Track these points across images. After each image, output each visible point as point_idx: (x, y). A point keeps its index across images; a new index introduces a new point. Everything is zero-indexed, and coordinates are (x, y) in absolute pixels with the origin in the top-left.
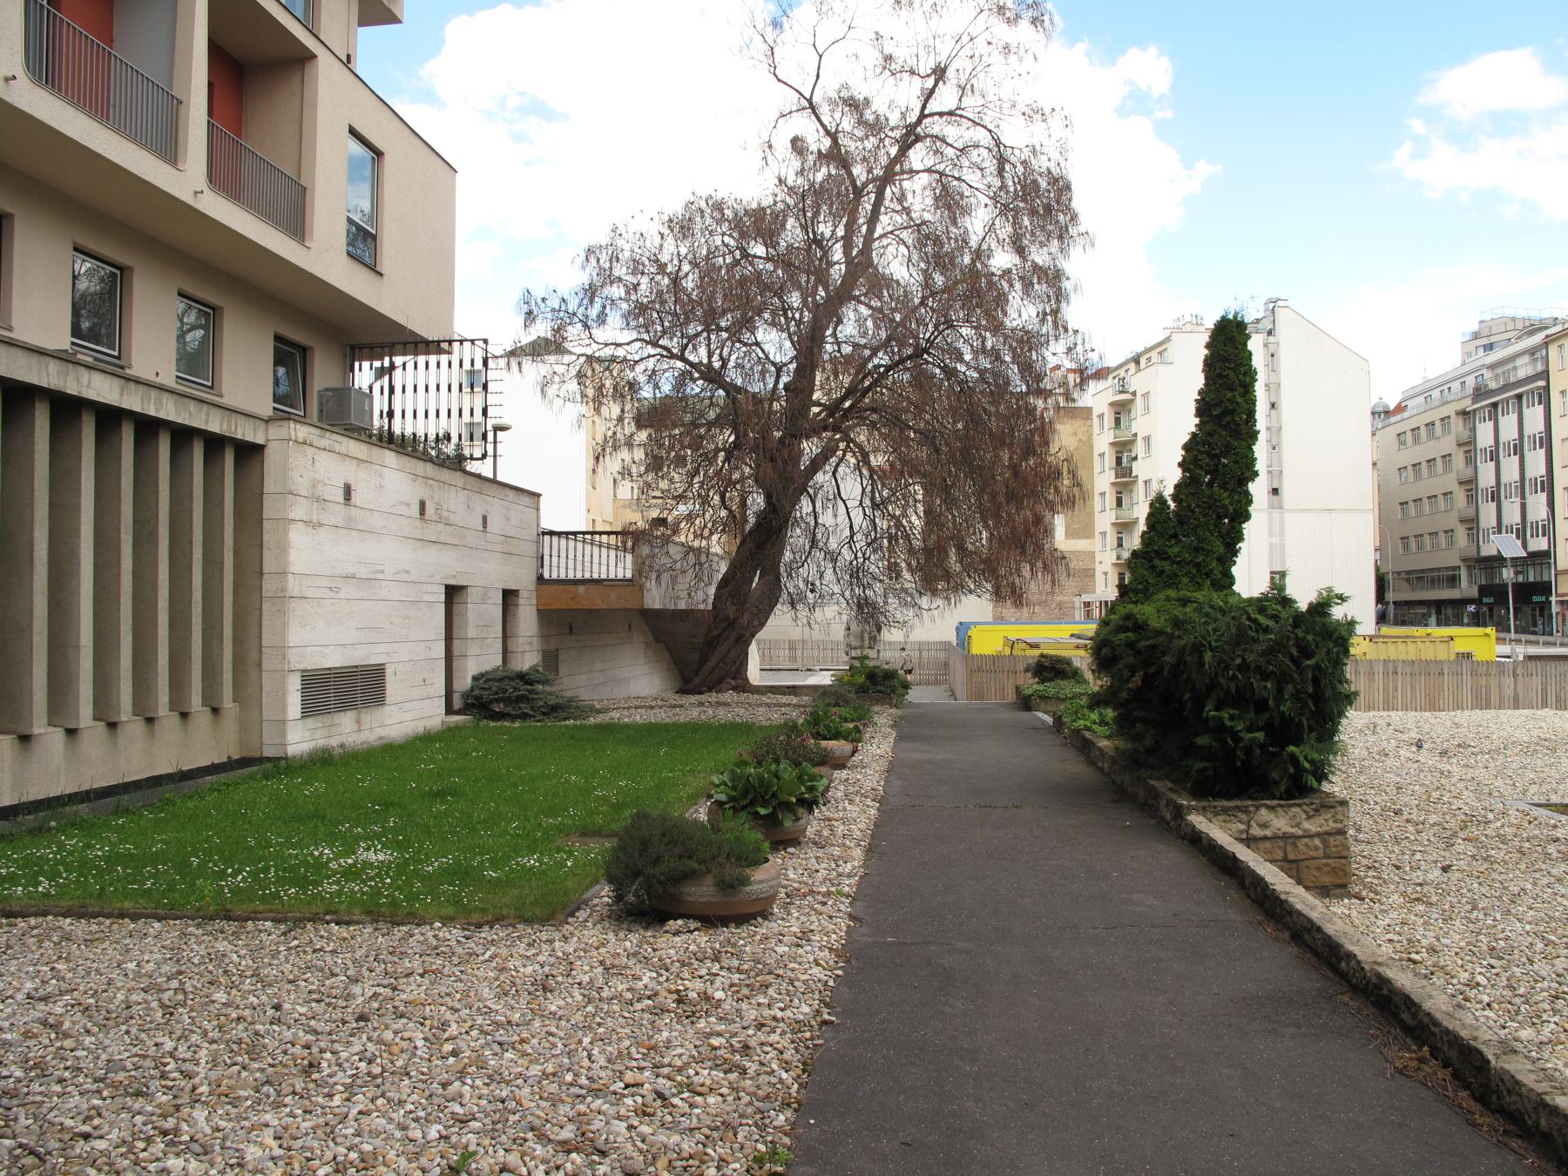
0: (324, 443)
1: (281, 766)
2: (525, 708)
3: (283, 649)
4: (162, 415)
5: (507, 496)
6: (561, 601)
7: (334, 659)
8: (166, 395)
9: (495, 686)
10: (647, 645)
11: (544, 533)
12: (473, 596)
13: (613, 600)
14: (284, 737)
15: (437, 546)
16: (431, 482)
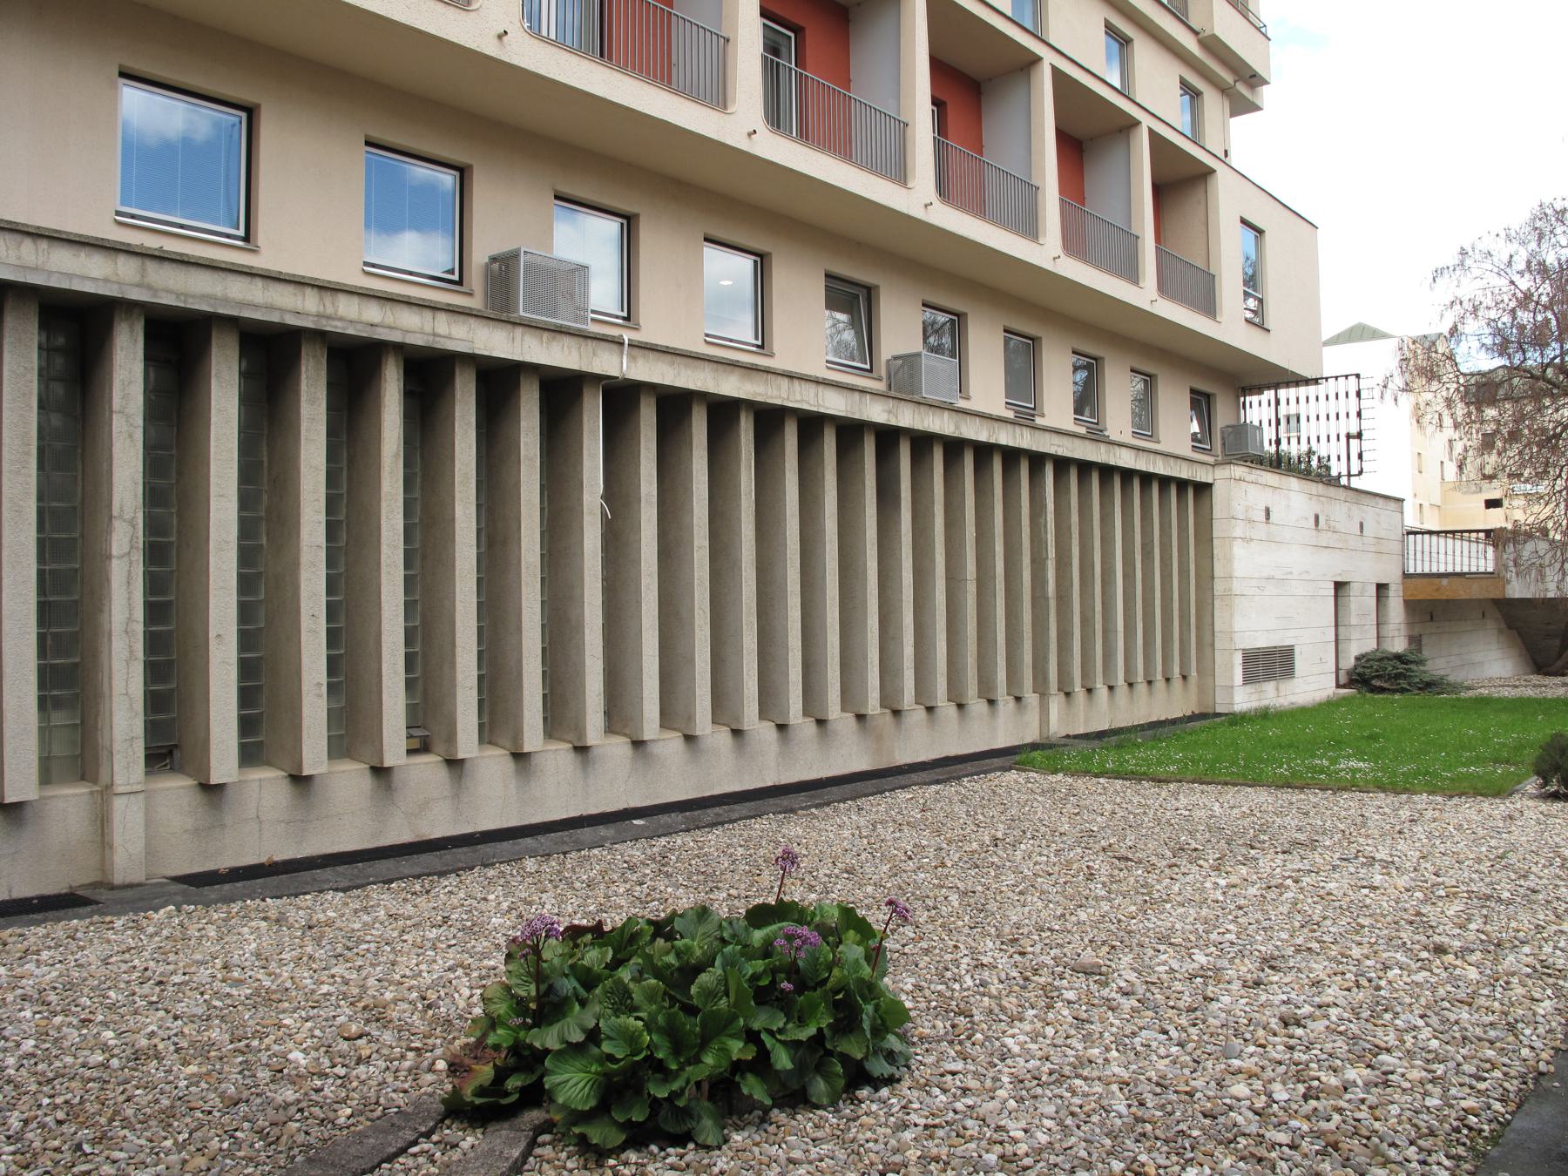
1: (1236, 719)
2: (1403, 684)
3: (1230, 634)
4: (1156, 472)
5: (1377, 503)
6: (1425, 592)
7: (1262, 642)
8: (1158, 456)
9: (1376, 665)
10: (1500, 631)
11: (1409, 533)
12: (1354, 589)
13: (1476, 591)
15: (1328, 550)
16: (1322, 499)
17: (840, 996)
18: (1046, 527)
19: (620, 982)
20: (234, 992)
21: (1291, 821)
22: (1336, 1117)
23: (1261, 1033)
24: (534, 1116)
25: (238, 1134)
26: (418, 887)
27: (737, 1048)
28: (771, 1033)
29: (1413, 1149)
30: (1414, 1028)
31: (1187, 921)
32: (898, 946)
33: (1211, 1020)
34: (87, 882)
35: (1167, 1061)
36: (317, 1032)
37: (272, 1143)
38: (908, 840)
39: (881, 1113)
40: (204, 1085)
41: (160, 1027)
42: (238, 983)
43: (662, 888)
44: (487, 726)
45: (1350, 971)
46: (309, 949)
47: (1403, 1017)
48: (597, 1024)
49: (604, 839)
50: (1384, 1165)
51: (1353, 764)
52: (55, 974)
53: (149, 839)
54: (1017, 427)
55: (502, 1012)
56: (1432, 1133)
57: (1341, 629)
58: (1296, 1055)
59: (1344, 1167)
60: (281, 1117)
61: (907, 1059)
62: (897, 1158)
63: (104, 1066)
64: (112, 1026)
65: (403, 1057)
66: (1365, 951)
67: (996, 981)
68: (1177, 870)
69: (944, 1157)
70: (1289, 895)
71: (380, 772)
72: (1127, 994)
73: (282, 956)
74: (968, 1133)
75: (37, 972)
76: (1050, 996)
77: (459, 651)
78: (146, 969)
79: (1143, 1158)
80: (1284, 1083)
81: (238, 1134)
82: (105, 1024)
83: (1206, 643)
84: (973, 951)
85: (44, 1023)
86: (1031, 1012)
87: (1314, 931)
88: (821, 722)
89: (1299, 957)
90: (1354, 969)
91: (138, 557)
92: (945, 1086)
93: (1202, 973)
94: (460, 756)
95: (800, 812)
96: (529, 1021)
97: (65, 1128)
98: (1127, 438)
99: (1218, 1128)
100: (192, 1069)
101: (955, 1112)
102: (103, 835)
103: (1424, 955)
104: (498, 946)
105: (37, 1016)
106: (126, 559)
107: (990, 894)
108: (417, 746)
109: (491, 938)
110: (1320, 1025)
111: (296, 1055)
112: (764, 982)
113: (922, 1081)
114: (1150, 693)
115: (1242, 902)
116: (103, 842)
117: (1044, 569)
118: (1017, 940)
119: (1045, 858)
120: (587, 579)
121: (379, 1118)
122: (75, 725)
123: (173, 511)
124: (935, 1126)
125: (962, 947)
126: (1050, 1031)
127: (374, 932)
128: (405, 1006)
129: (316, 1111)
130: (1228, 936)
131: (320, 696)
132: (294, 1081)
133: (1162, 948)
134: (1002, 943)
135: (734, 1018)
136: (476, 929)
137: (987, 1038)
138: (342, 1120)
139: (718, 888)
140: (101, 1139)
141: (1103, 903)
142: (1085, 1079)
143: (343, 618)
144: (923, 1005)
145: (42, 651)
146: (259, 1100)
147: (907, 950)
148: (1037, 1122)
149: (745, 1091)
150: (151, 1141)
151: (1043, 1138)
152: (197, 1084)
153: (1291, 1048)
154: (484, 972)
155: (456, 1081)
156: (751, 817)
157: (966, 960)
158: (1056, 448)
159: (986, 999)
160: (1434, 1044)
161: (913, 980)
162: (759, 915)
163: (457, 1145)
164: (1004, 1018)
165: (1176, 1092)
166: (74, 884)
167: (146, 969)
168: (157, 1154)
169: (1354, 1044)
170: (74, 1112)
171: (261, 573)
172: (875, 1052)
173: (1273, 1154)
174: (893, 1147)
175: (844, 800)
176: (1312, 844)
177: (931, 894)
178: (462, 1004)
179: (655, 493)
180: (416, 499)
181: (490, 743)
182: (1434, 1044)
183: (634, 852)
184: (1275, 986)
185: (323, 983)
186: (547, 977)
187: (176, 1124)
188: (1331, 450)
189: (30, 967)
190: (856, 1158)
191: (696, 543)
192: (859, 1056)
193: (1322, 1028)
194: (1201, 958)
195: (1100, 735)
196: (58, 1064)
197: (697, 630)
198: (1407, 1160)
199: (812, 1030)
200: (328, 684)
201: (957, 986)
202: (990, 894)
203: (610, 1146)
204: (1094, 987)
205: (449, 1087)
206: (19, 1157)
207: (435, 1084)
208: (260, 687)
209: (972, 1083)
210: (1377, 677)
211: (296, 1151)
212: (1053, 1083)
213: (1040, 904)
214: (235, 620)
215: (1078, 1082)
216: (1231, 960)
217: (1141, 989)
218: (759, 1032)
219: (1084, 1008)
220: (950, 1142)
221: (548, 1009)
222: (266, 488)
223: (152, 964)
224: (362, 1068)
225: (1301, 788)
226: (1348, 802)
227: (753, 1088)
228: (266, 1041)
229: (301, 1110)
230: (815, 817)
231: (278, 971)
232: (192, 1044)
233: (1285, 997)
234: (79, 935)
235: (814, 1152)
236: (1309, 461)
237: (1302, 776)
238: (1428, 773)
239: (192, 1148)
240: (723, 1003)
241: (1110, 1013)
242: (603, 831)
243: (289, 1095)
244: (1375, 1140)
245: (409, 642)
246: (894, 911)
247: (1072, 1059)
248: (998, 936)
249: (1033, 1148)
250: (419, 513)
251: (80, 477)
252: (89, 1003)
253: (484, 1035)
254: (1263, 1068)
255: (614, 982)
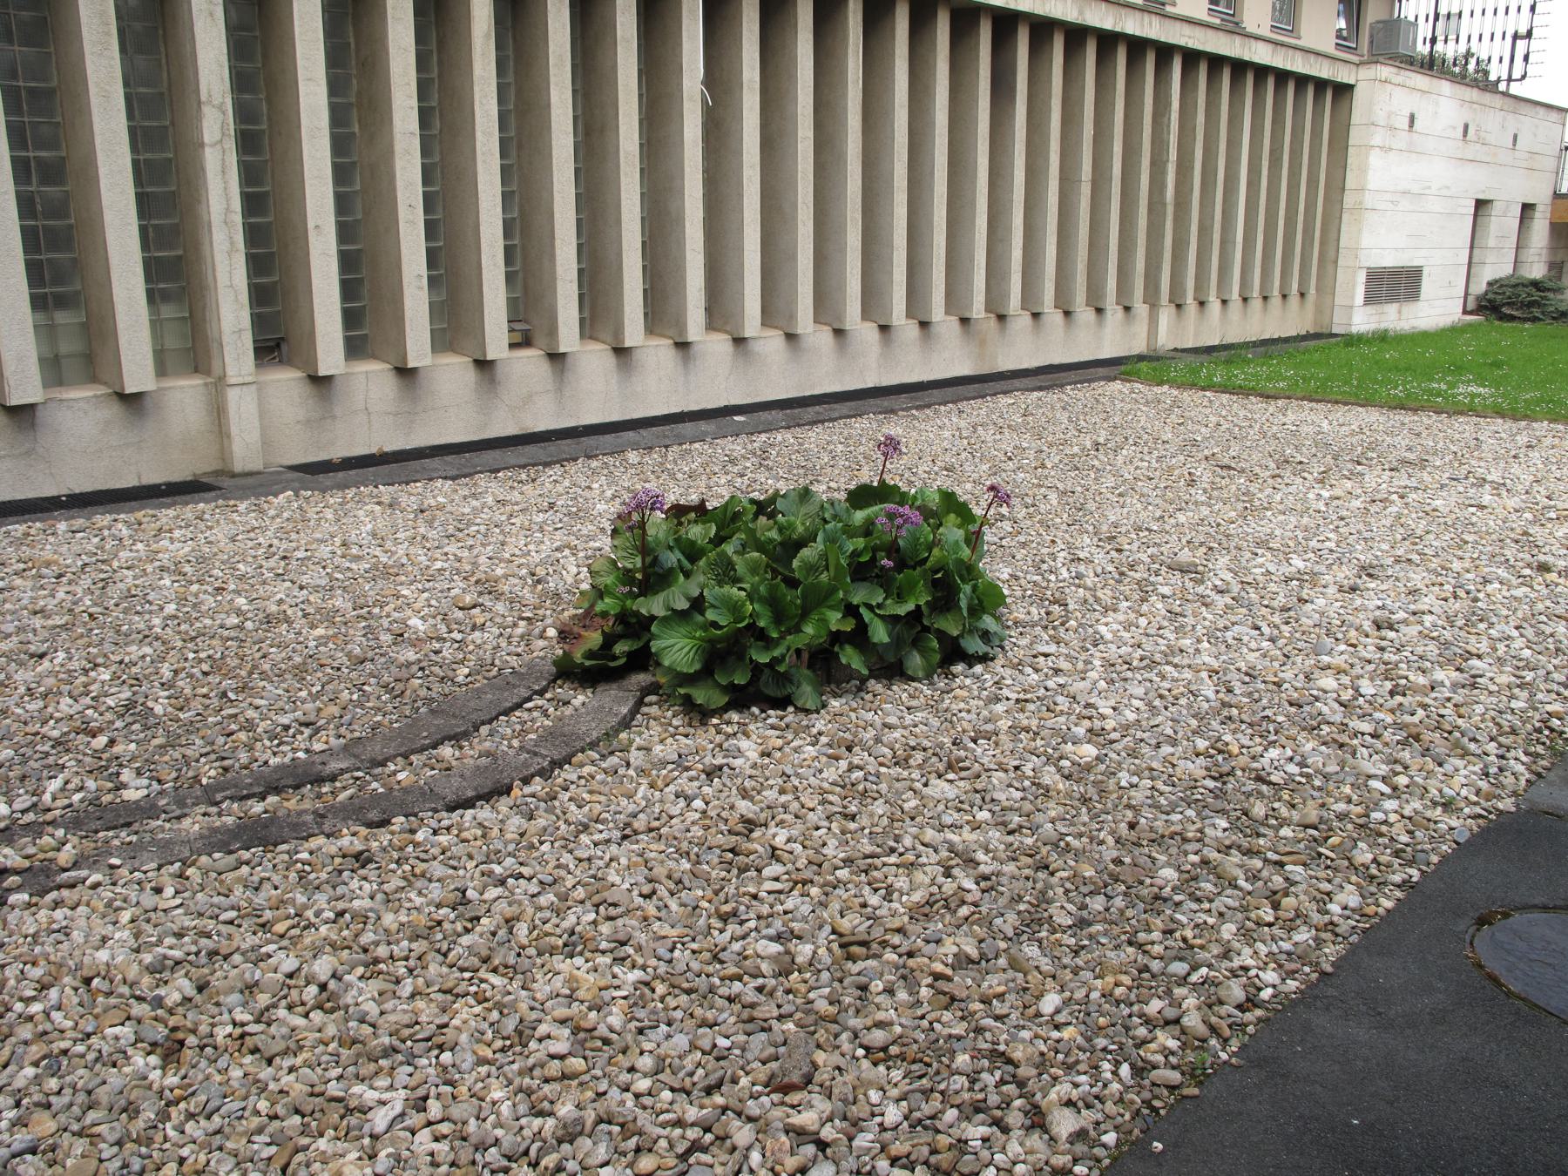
0: (1399, 79)
1: (1351, 340)
2: (1536, 312)
3: (1355, 252)
4: (1294, 69)
7: (1389, 261)
9: (1509, 291)
12: (1497, 209)
14: (1350, 318)
17: (939, 575)
18: (1169, 126)
19: (724, 553)
20: (354, 566)
21: (1402, 441)
22: (1421, 713)
23: (1353, 633)
24: (642, 679)
25: (366, 688)
26: (524, 476)
27: (835, 620)
28: (870, 607)
29: (1493, 744)
30: (1509, 638)
31: (1287, 528)
32: (996, 539)
33: (1304, 620)
34: (209, 470)
35: (1257, 654)
36: (433, 602)
37: (398, 696)
38: (1008, 442)
39: (975, 687)
40: (331, 645)
41: (288, 596)
42: (357, 558)
43: (763, 480)
44: (588, 322)
45: (1448, 583)
46: (422, 530)
47: (1497, 627)
48: (702, 593)
49: (706, 434)
50: (1462, 757)
51: (1473, 389)
52: (187, 549)
53: (264, 429)
54: (1146, 14)
55: (609, 582)
56: (1514, 732)
57: (1476, 251)
58: (1386, 656)
59: (1423, 756)
60: (404, 674)
61: (1002, 640)
62: (989, 727)
63: (240, 627)
64: (243, 594)
65: (515, 625)
66: (1467, 565)
67: (1092, 575)
68: (1279, 480)
69: (1034, 728)
70: (1393, 509)
71: (484, 365)
72: (1221, 592)
73: (398, 536)
74: (1058, 708)
75: (171, 547)
76: (1145, 591)
77: (558, 243)
78: (271, 546)
79: (1227, 738)
80: (1372, 679)
81: (366, 688)
82: (238, 592)
83: (1329, 261)
84: (1070, 547)
85: (182, 590)
86: (1126, 604)
87: (1416, 544)
88: (924, 325)
89: (1397, 567)
90: (1453, 581)
91: (231, 145)
92: (1038, 666)
93: (1300, 577)
94: (562, 350)
95: (900, 413)
96: (635, 590)
97: (210, 678)
98: (1265, 31)
99: (1303, 716)
100: (320, 631)
101: (1047, 689)
102: (220, 425)
103: (1527, 572)
104: (603, 530)
105: (176, 584)
106: (218, 147)
107: (1089, 495)
108: (520, 340)
109: (596, 522)
110: (1413, 630)
111: (415, 622)
112: (865, 558)
113: (1016, 661)
114: (1265, 309)
115: (1345, 513)
116: (221, 432)
117: (1164, 173)
118: (1115, 537)
119: (1146, 464)
120: (687, 170)
121: (495, 677)
122: (184, 318)
123: (261, 96)
124: (1026, 701)
125: (1059, 542)
126: (1143, 622)
127: (483, 516)
128: (515, 581)
129: (436, 669)
130: (1327, 544)
131: (421, 288)
132: (416, 643)
133: (1260, 551)
134: (1100, 540)
135: (834, 590)
136: (582, 514)
137: (1081, 625)
138: (460, 679)
139: (818, 481)
140: (242, 689)
141: (1203, 508)
142: (1176, 666)
143: (440, 210)
144: (1019, 593)
145: (145, 245)
146: (383, 660)
147: (1004, 542)
148: (1126, 701)
149: (844, 661)
150: (288, 691)
151: (1132, 716)
152: (325, 645)
153: (1382, 649)
154: (590, 553)
155: (566, 647)
156: (854, 416)
157: (1063, 554)
158: (1186, 39)
159: (1081, 590)
160: (1527, 653)
161: (1010, 571)
162: (862, 496)
163: (569, 703)
164: (1098, 608)
165: (1264, 682)
166: (198, 472)
167: (271, 546)
168: (294, 702)
169: (1446, 649)
170: (217, 665)
171: (355, 163)
172: (970, 632)
173: (1355, 742)
174: (985, 718)
175: (945, 403)
176: (1423, 463)
177: (1030, 493)
178: (570, 580)
179: (758, 79)
180: (509, 84)
181: (591, 338)
182: (1527, 653)
183: (736, 446)
184: (1372, 593)
185: (437, 560)
186: (653, 550)
187: (309, 678)
188: (1495, 54)
189: (165, 543)
190: (949, 725)
191: (800, 134)
192: (955, 633)
193: (1415, 633)
194: (1298, 563)
195: (1210, 350)
196: (198, 625)
197: (800, 226)
198: (1485, 754)
199: (910, 606)
200: (429, 277)
201: (1053, 578)
202: (1089, 495)
203: (714, 707)
204: (1189, 585)
205: (560, 652)
206: (173, 701)
207: (546, 648)
208: (362, 280)
209: (1064, 665)
210: (1508, 304)
211: (420, 703)
212: (1144, 668)
213: (1139, 505)
214: (328, 153)
215: (1168, 668)
216: (1329, 567)
217: (1236, 588)
218: (858, 606)
219: (1178, 602)
220: (1040, 715)
221: (653, 579)
222: (354, 72)
223: (275, 542)
224: (477, 634)
225: (1415, 411)
226: (1463, 427)
227: (851, 658)
228: (386, 609)
229: (422, 669)
230: (915, 418)
231: (394, 549)
232: (318, 610)
233: (1380, 603)
234: (207, 516)
235: (908, 719)
236: (1466, 63)
237: (1416, 398)
238: (1551, 401)
239: (325, 698)
240: (824, 577)
241: (1204, 608)
242: (703, 426)
243: (411, 655)
244: (1457, 734)
245: (507, 233)
246: (995, 497)
247: (1163, 648)
248: (1095, 534)
249: (1120, 724)
250: (513, 98)
251: (164, 61)
252: (221, 574)
253: (592, 606)
254: (1352, 665)
255: (718, 554)
